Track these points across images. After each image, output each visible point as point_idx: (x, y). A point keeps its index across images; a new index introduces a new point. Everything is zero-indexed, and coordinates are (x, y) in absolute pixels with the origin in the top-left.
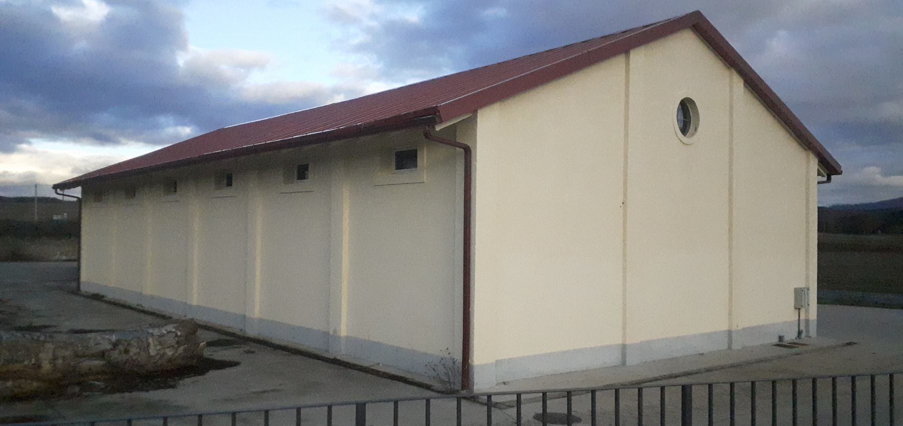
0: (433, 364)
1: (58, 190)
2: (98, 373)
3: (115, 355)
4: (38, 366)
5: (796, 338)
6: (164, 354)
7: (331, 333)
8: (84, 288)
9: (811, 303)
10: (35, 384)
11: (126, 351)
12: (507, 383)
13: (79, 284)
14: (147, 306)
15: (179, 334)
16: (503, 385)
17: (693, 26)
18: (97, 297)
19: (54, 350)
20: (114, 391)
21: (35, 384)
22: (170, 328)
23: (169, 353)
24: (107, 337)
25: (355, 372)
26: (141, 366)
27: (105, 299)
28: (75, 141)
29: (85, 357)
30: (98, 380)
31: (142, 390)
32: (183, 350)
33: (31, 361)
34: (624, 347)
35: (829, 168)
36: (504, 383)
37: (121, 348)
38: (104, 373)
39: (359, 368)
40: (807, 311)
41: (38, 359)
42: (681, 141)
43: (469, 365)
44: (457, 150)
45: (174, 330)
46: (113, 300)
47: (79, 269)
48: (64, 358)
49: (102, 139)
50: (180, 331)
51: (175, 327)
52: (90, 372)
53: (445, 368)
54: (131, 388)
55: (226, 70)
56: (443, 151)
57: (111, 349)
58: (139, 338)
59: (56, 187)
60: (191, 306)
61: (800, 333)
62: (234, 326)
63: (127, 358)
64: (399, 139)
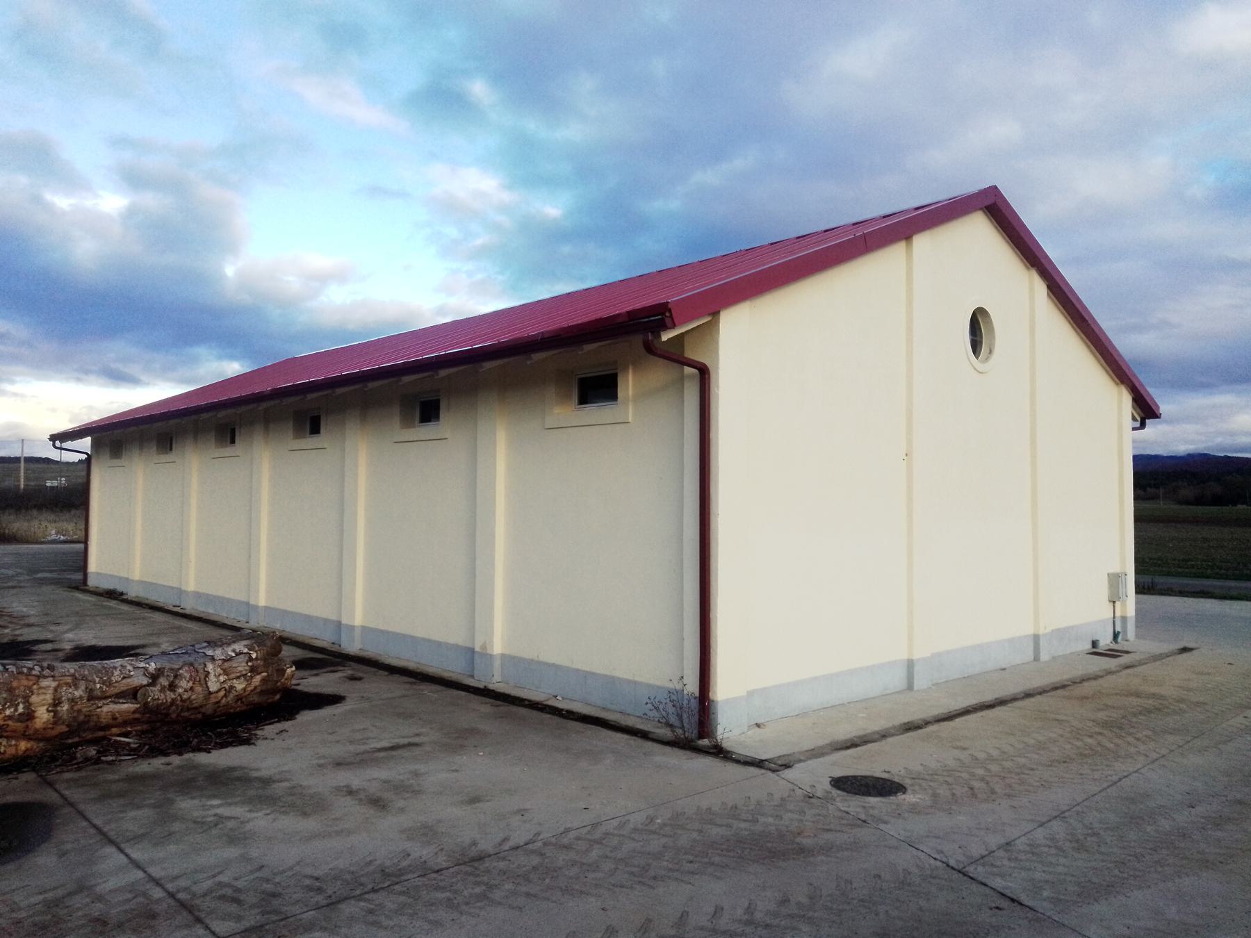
0: (657, 700)
1: (58, 443)
2: (125, 723)
3: (156, 694)
4: (29, 716)
5: (1111, 643)
6: (232, 687)
7: (477, 649)
8: (92, 582)
9: (1129, 594)
10: (23, 745)
11: (172, 687)
12: (762, 726)
13: (85, 575)
14: (189, 606)
15: (254, 656)
16: (757, 729)
17: (987, 208)
18: (112, 595)
19: (56, 690)
20: (155, 752)
21: (23, 745)
22: (240, 646)
23: (240, 685)
24: (142, 665)
25: (524, 711)
26: (196, 708)
27: (125, 597)
28: (79, 380)
29: (106, 698)
30: (126, 735)
31: (198, 749)
32: (261, 681)
33: (16, 710)
34: (910, 665)
35: (1146, 411)
36: (758, 726)
37: (164, 681)
38: (135, 721)
39: (527, 703)
40: (1124, 606)
41: (28, 704)
42: (975, 369)
43: (711, 702)
44: (685, 370)
45: (246, 650)
46: (136, 600)
47: (86, 551)
48: (73, 701)
49: (117, 377)
50: (256, 652)
51: (246, 646)
52: (115, 721)
53: (674, 706)
54: (181, 747)
55: (292, 283)
56: (659, 373)
57: (149, 685)
58: (191, 664)
59: (54, 438)
60: (256, 607)
61: (1116, 636)
62: (324, 638)
63: (173, 696)
64: (590, 356)
